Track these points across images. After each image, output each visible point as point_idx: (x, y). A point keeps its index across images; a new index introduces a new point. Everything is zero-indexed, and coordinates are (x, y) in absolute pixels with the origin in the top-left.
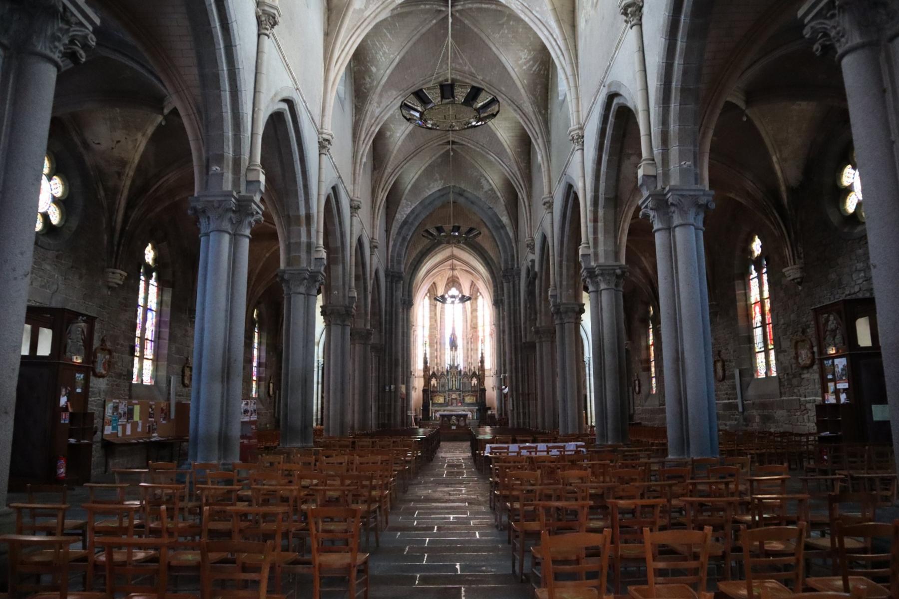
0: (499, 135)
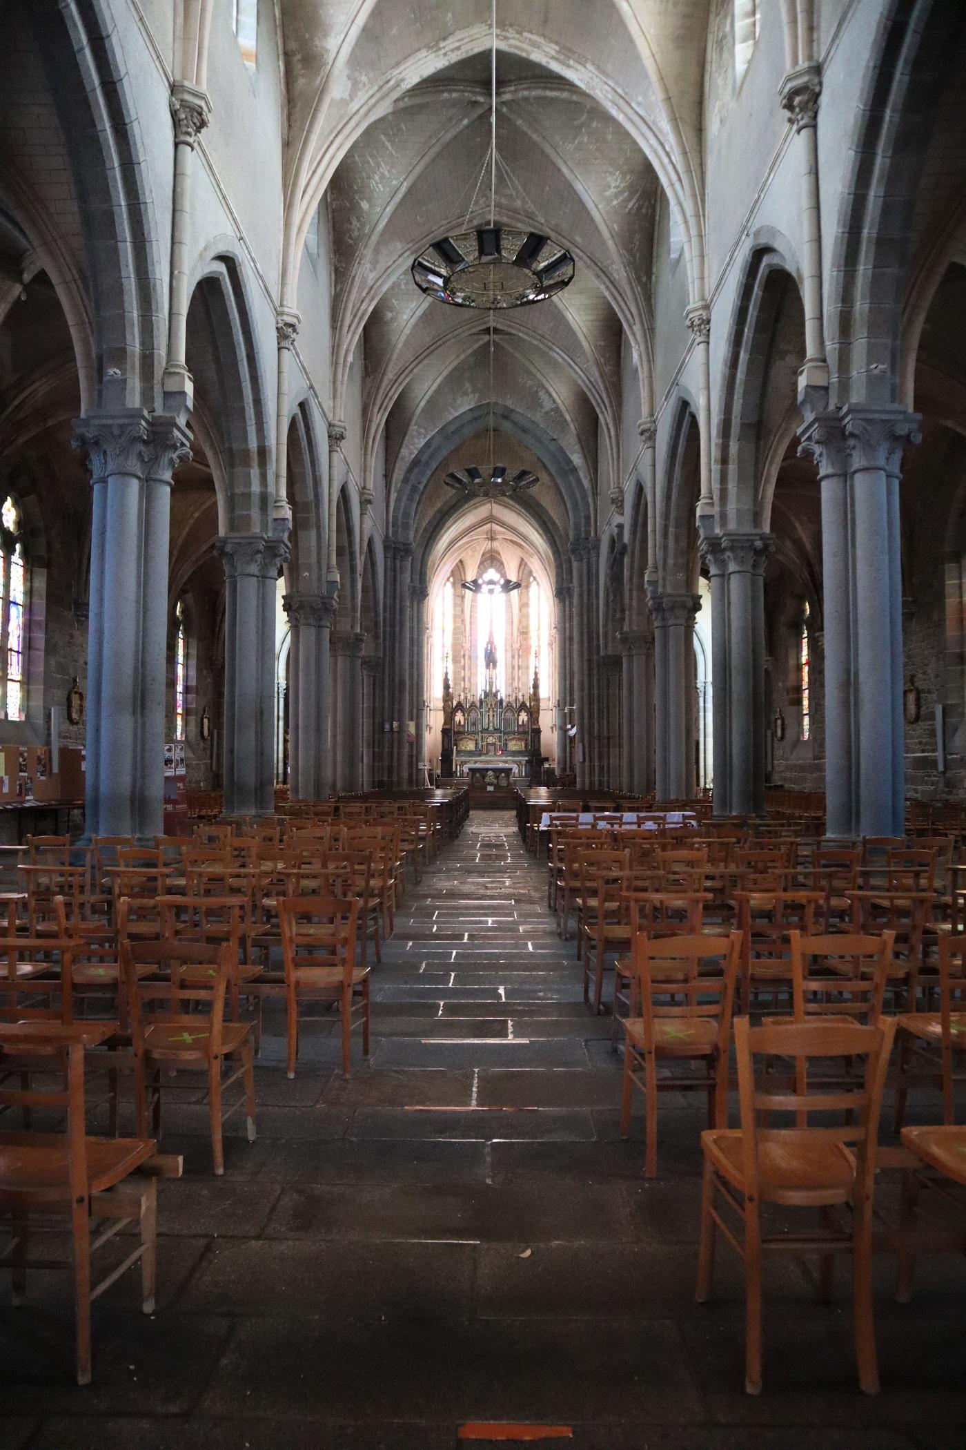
0: (570, 318)
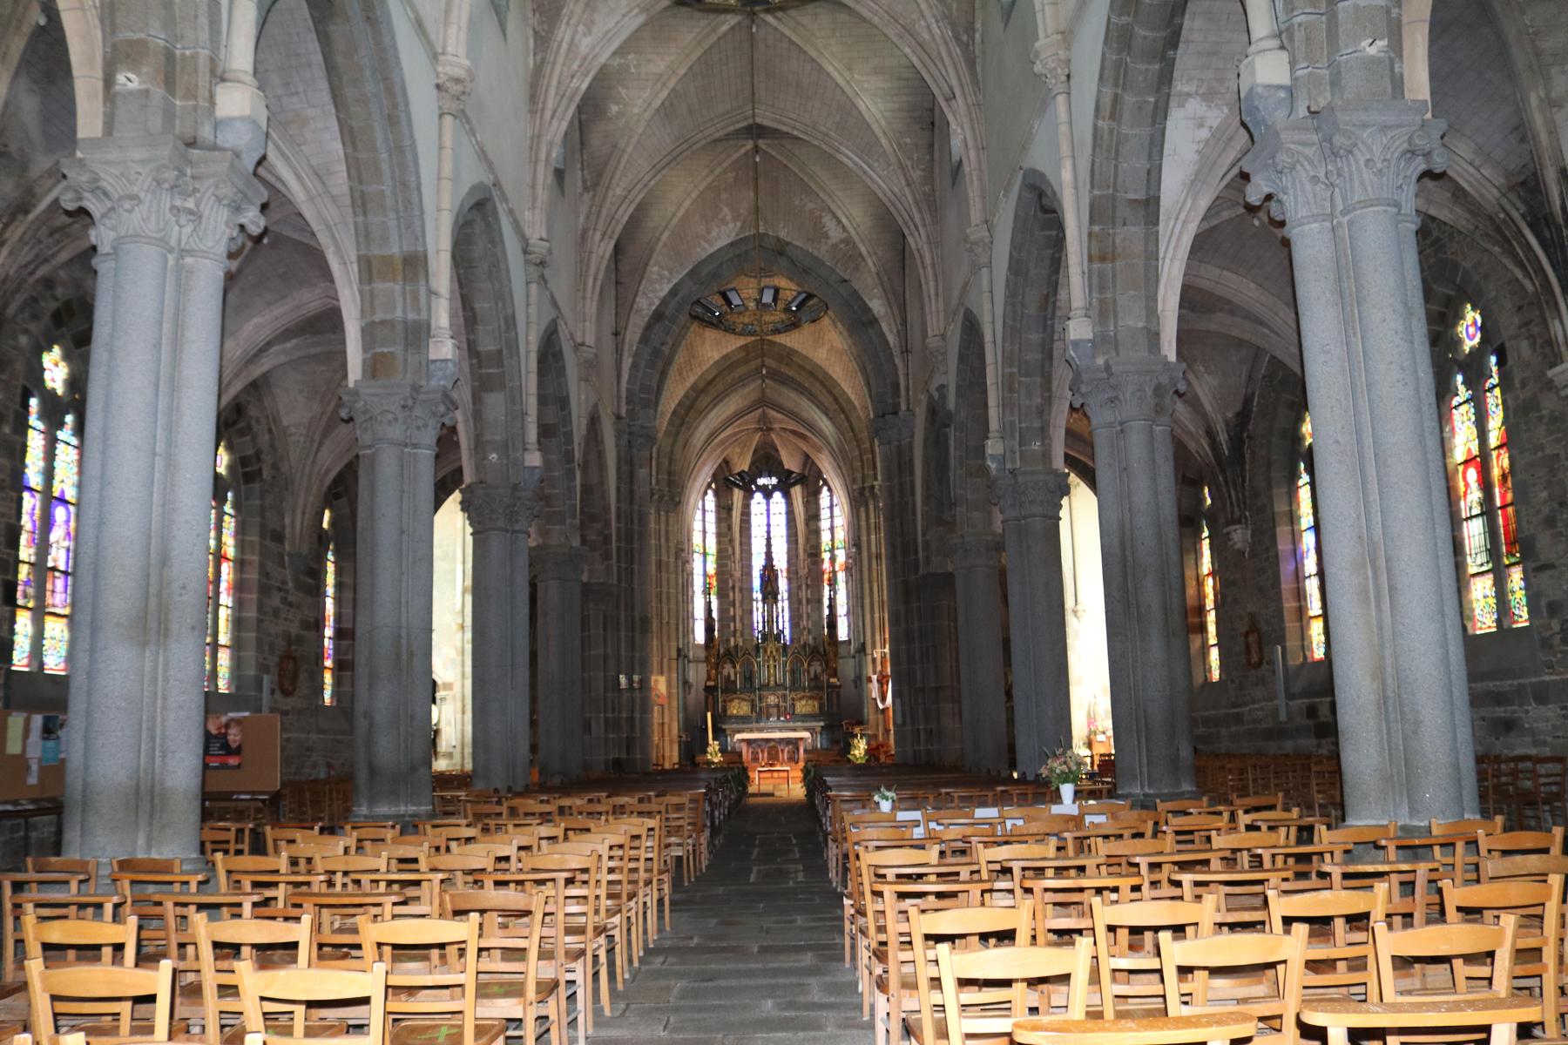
0: (862, 107)
